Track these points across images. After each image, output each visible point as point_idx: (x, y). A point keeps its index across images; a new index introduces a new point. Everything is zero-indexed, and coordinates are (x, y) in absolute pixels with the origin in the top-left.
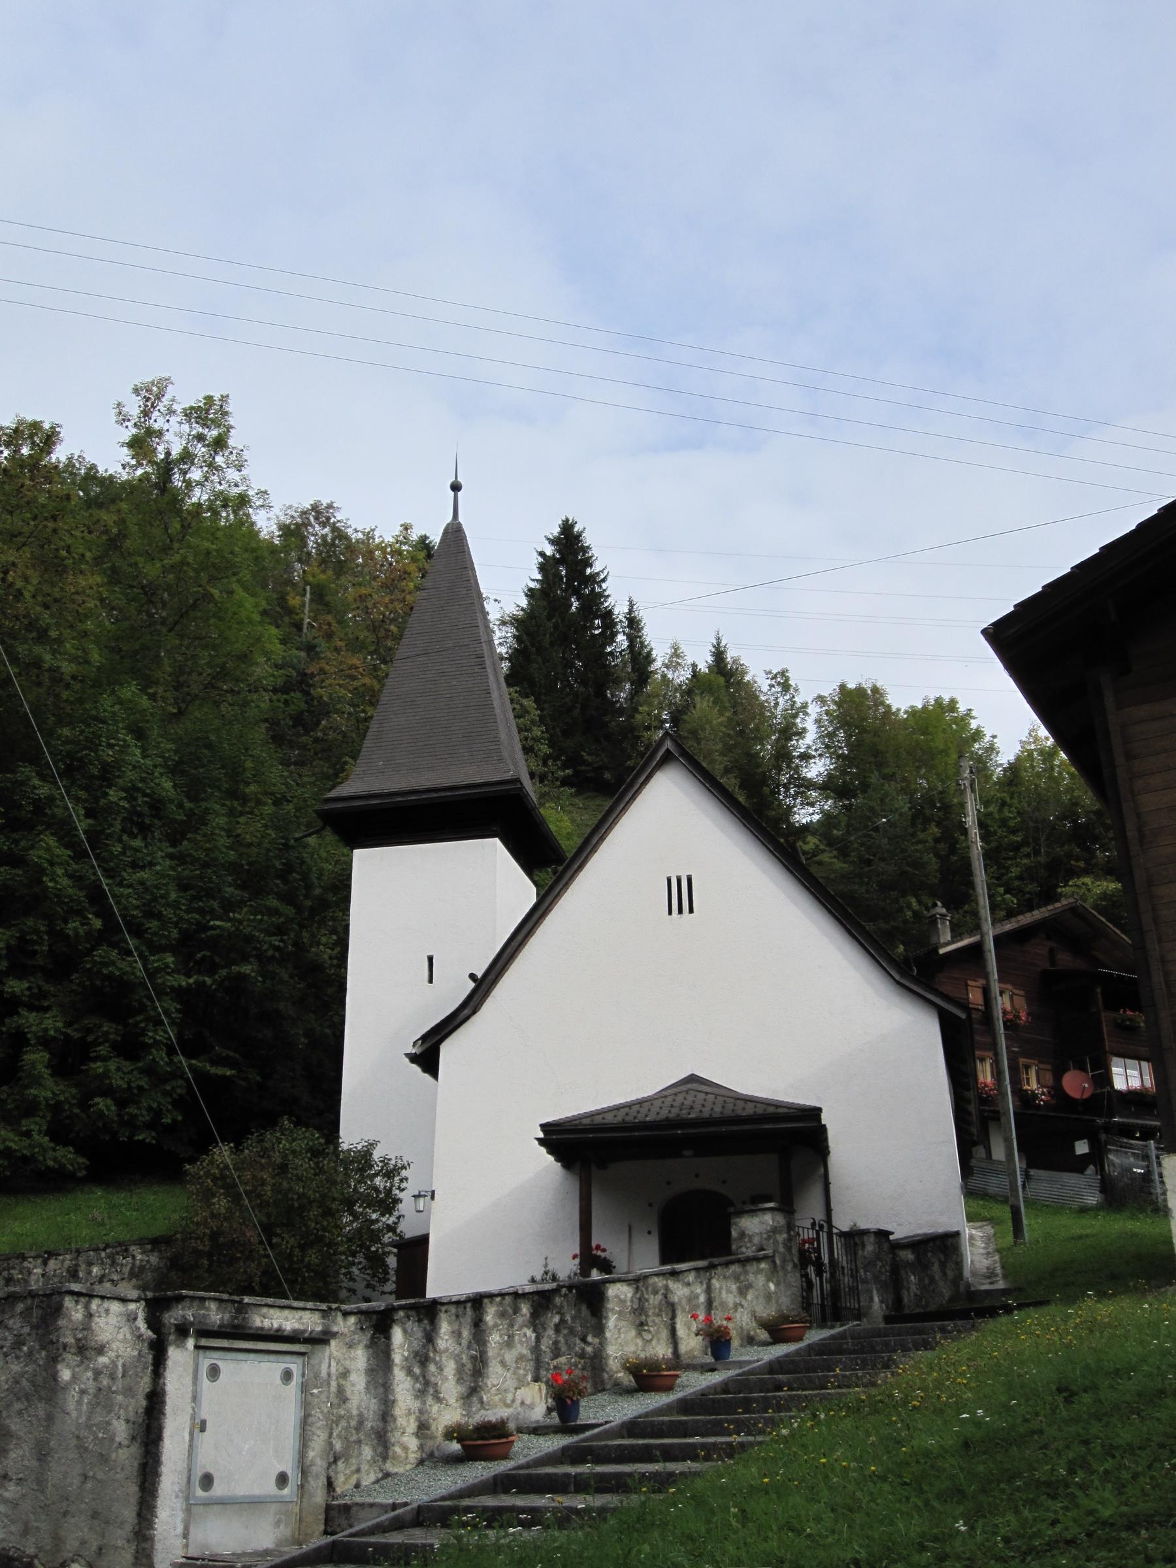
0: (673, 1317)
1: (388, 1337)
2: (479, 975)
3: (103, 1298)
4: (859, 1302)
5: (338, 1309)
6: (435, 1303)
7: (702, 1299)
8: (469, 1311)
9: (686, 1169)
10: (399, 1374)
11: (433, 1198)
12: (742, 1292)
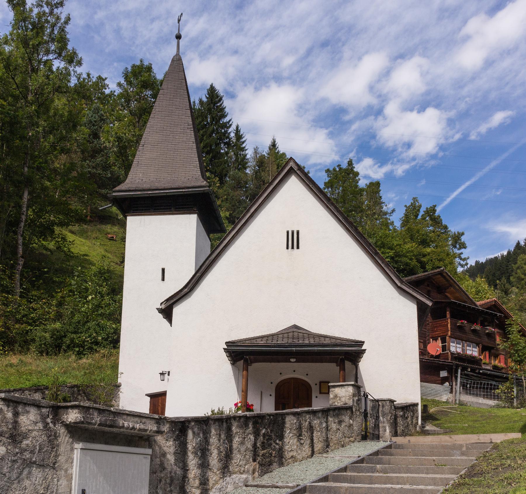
0: (312, 433)
1: (186, 435)
3: (25, 404)
4: (379, 431)
8: (225, 425)
10: (191, 456)
11: (169, 375)
12: (340, 422)
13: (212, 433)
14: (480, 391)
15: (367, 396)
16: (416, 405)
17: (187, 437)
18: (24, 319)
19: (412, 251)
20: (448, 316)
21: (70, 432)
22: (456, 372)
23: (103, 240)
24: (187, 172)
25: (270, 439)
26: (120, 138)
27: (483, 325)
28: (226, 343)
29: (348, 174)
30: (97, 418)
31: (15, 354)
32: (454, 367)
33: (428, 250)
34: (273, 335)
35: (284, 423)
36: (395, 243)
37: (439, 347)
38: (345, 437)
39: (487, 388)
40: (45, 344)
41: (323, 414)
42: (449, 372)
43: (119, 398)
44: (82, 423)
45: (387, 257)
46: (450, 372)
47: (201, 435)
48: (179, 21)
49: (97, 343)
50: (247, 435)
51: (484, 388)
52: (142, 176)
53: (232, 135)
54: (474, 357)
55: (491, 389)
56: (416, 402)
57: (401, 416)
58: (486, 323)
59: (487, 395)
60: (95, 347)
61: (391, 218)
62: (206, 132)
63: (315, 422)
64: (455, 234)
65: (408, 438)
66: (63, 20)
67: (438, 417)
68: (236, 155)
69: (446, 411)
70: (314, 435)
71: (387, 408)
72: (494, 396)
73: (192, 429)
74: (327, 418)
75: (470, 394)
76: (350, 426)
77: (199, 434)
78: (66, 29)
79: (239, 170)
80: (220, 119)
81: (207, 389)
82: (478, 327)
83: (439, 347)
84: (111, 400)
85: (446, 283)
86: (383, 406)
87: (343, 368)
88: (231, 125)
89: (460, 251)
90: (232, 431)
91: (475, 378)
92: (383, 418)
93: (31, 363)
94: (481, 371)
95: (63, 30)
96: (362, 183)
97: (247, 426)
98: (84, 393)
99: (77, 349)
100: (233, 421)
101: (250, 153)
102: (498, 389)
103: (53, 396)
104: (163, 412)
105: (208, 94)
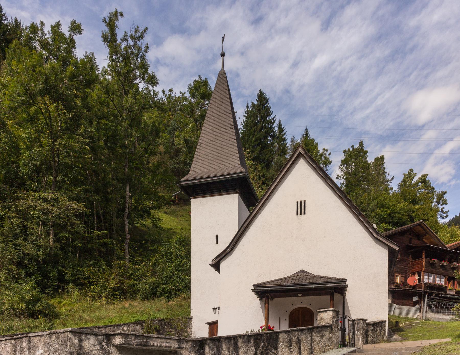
0: (300, 344)
2: (222, 332)
3: (86, 334)
5: (184, 339)
6: (220, 338)
8: (233, 341)
11: (219, 309)
12: (322, 336)
13: (223, 347)
14: (440, 310)
15: (346, 317)
17: (204, 350)
18: (132, 276)
19: (404, 209)
21: (119, 350)
22: (424, 297)
23: (186, 217)
25: (267, 349)
27: (450, 261)
28: (253, 285)
29: (359, 152)
30: (134, 341)
31: (127, 301)
32: (423, 294)
33: (417, 207)
34: (285, 278)
35: (278, 338)
38: (326, 346)
40: (146, 293)
41: (308, 331)
42: (419, 297)
43: (192, 326)
44: (124, 344)
46: (420, 297)
47: (215, 349)
48: (223, 41)
49: (180, 290)
50: (251, 347)
51: (443, 307)
52: (202, 167)
53: (276, 129)
55: (448, 308)
58: (452, 260)
61: (391, 184)
62: (256, 128)
63: (303, 337)
65: (374, 345)
67: (405, 329)
70: (301, 345)
71: (361, 325)
72: (450, 313)
73: (208, 345)
74: (312, 334)
75: (433, 312)
76: (330, 338)
77: (213, 348)
79: (281, 156)
80: (267, 117)
81: (243, 316)
82: (445, 263)
83: (415, 279)
84: (186, 328)
85: (424, 231)
86: (358, 324)
87: (332, 299)
88: (275, 121)
89: (443, 206)
92: (358, 332)
93: (136, 306)
94: (443, 296)
95: (144, 59)
96: (370, 160)
97: (249, 341)
98: (169, 324)
99: (167, 295)
101: (289, 143)
102: (453, 307)
103: (148, 327)
105: (258, 98)
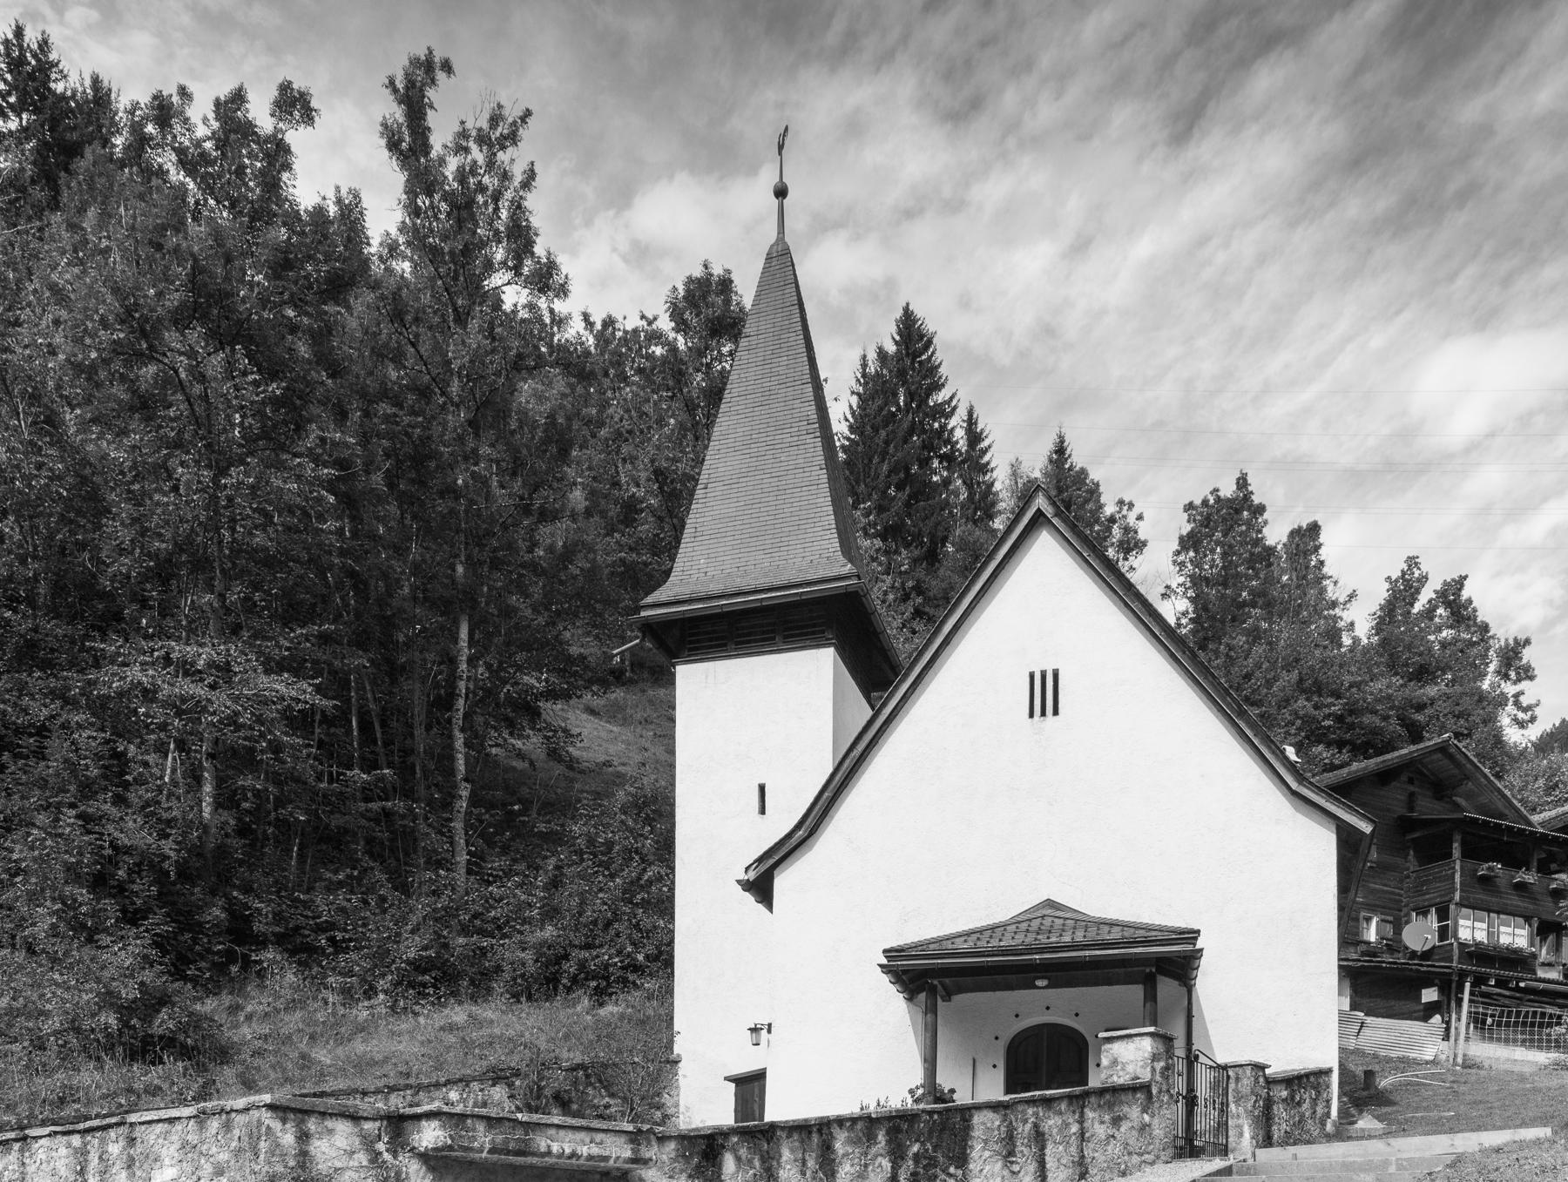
0: (1043, 1148)
3: (323, 1114)
5: (650, 1131)
6: (773, 1126)
7: (1074, 1128)
8: (815, 1138)
9: (1047, 1001)
11: (769, 1031)
12: (1116, 1121)
13: (784, 1159)
14: (1515, 1032)
15: (1197, 1057)
16: (1328, 1072)
17: (720, 1168)
18: (477, 922)
19: (1389, 697)
20: (1456, 853)
21: (431, 1169)
22: (1461, 989)
24: (806, 544)
25: (933, 1163)
26: (662, 473)
28: (885, 951)
29: (1238, 511)
31: (460, 1003)
33: (1432, 691)
36: (1347, 679)
37: (1430, 931)
38: (1130, 1154)
39: (1533, 1024)
41: (1070, 1104)
42: (1441, 991)
44: (450, 1148)
45: (1327, 717)
46: (1445, 989)
47: (757, 1163)
51: (1524, 1024)
52: (713, 559)
53: (959, 434)
54: (1517, 951)
55: (1541, 1025)
56: (1325, 1066)
57: (1284, 1100)
58: (1554, 866)
59: (1532, 1041)
60: (631, 977)
61: (1345, 615)
63: (1051, 1122)
64: (1507, 645)
66: (518, 178)
68: (969, 485)
69: (1419, 1084)
70: (1048, 1151)
71: (1246, 1083)
72: (1549, 1041)
73: (734, 1151)
74: (1082, 1114)
75: (1491, 1039)
76: (1144, 1128)
77: (750, 1162)
78: (526, 203)
79: (975, 522)
80: (928, 395)
81: (852, 1055)
82: (1530, 877)
85: (1456, 771)
86: (1238, 1079)
87: (1151, 996)
88: (955, 408)
89: (1518, 688)
90: (834, 1152)
91: (1507, 1002)
93: (492, 1022)
94: (1522, 985)
95: (519, 207)
97: (871, 1138)
98: (600, 1081)
99: (593, 984)
100: (836, 1130)
101: (1001, 479)
102: (1558, 1024)
104: (762, 1117)
105: (900, 333)
